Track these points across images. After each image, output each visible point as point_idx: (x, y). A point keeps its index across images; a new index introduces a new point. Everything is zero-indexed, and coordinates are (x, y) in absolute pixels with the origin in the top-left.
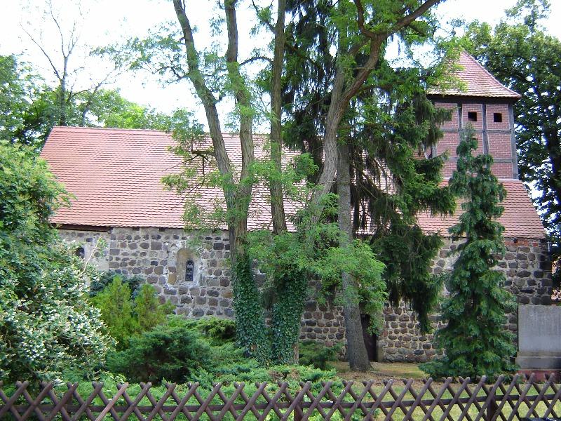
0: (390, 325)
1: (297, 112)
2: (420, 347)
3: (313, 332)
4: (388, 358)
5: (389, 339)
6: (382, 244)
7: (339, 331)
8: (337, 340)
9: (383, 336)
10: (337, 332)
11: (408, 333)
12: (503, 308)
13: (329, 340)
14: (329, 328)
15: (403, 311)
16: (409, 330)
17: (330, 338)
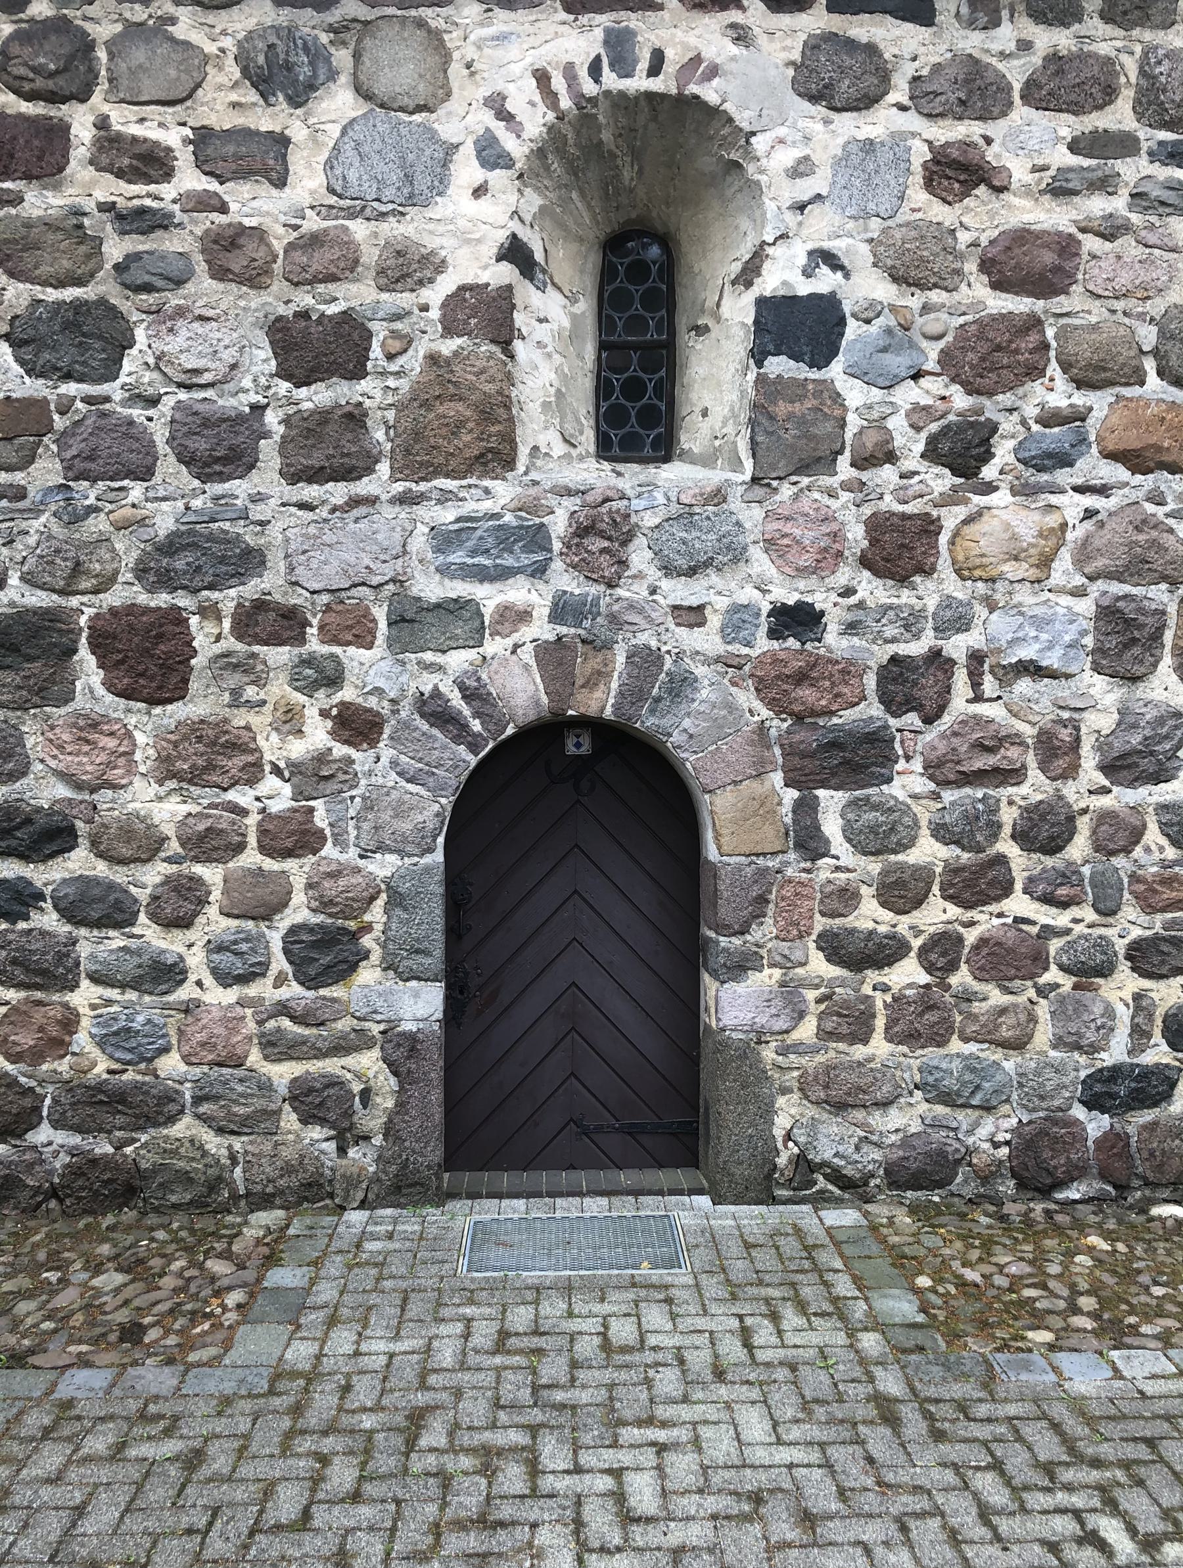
0: (832, 826)
1: (945, 358)
2: (1140, 1034)
3: (48, 919)
4: (825, 1152)
5: (819, 966)
6: (906, 452)
7: (324, 905)
8: (294, 990)
9: (765, 932)
10: (299, 911)
11: (1019, 904)
12: (1009, 248)
13: (219, 996)
14: (211, 874)
15: (961, 681)
16: (1020, 862)
17: (225, 979)
